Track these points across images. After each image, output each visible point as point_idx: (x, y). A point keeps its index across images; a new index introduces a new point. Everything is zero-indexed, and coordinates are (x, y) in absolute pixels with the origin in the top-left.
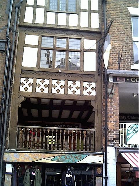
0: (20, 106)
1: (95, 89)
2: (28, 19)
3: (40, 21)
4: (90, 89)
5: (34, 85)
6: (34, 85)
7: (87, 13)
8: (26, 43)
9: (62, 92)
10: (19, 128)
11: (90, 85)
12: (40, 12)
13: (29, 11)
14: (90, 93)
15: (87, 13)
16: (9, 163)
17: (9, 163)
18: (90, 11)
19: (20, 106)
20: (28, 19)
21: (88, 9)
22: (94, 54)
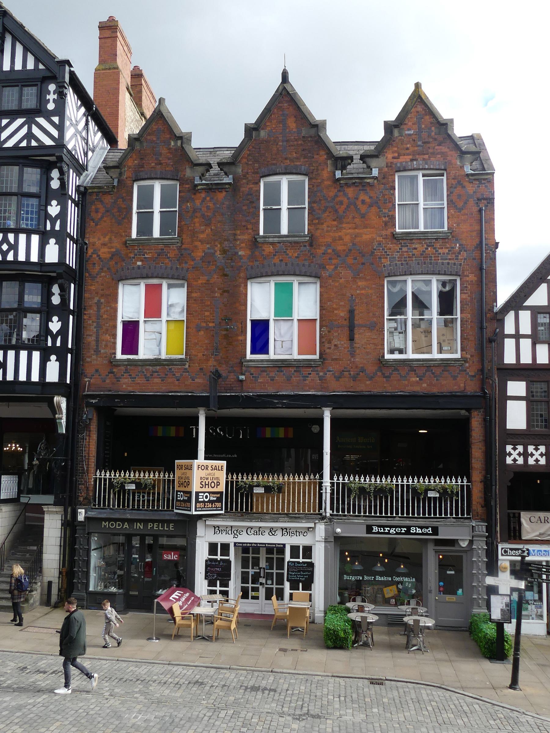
0: (509, 484)
1: (545, 455)
2: (509, 358)
3: (526, 359)
4: (537, 455)
5: (525, 455)
6: (525, 455)
7: (513, 341)
8: (509, 393)
9: (520, 461)
10: (509, 514)
11: (515, 449)
12: (526, 344)
13: (509, 345)
14: (537, 460)
15: (513, 341)
16: (149, 535)
17: (149, 535)
18: (517, 336)
19: (509, 484)
20: (509, 358)
21: (514, 333)
22: (523, 404)
